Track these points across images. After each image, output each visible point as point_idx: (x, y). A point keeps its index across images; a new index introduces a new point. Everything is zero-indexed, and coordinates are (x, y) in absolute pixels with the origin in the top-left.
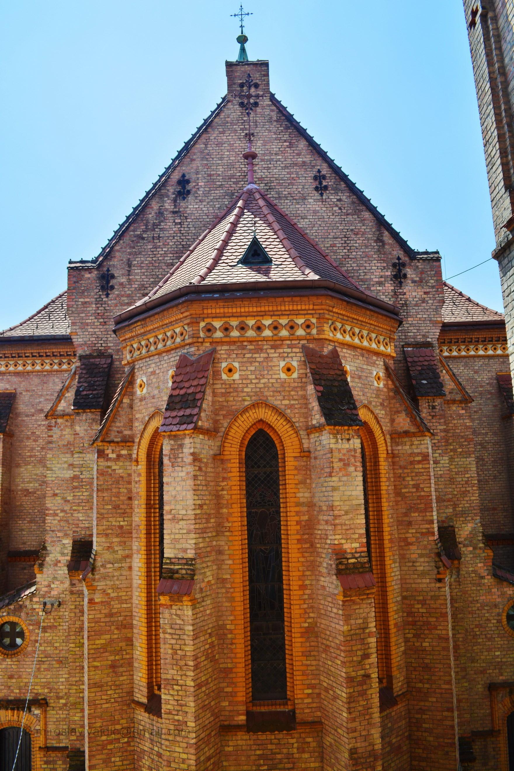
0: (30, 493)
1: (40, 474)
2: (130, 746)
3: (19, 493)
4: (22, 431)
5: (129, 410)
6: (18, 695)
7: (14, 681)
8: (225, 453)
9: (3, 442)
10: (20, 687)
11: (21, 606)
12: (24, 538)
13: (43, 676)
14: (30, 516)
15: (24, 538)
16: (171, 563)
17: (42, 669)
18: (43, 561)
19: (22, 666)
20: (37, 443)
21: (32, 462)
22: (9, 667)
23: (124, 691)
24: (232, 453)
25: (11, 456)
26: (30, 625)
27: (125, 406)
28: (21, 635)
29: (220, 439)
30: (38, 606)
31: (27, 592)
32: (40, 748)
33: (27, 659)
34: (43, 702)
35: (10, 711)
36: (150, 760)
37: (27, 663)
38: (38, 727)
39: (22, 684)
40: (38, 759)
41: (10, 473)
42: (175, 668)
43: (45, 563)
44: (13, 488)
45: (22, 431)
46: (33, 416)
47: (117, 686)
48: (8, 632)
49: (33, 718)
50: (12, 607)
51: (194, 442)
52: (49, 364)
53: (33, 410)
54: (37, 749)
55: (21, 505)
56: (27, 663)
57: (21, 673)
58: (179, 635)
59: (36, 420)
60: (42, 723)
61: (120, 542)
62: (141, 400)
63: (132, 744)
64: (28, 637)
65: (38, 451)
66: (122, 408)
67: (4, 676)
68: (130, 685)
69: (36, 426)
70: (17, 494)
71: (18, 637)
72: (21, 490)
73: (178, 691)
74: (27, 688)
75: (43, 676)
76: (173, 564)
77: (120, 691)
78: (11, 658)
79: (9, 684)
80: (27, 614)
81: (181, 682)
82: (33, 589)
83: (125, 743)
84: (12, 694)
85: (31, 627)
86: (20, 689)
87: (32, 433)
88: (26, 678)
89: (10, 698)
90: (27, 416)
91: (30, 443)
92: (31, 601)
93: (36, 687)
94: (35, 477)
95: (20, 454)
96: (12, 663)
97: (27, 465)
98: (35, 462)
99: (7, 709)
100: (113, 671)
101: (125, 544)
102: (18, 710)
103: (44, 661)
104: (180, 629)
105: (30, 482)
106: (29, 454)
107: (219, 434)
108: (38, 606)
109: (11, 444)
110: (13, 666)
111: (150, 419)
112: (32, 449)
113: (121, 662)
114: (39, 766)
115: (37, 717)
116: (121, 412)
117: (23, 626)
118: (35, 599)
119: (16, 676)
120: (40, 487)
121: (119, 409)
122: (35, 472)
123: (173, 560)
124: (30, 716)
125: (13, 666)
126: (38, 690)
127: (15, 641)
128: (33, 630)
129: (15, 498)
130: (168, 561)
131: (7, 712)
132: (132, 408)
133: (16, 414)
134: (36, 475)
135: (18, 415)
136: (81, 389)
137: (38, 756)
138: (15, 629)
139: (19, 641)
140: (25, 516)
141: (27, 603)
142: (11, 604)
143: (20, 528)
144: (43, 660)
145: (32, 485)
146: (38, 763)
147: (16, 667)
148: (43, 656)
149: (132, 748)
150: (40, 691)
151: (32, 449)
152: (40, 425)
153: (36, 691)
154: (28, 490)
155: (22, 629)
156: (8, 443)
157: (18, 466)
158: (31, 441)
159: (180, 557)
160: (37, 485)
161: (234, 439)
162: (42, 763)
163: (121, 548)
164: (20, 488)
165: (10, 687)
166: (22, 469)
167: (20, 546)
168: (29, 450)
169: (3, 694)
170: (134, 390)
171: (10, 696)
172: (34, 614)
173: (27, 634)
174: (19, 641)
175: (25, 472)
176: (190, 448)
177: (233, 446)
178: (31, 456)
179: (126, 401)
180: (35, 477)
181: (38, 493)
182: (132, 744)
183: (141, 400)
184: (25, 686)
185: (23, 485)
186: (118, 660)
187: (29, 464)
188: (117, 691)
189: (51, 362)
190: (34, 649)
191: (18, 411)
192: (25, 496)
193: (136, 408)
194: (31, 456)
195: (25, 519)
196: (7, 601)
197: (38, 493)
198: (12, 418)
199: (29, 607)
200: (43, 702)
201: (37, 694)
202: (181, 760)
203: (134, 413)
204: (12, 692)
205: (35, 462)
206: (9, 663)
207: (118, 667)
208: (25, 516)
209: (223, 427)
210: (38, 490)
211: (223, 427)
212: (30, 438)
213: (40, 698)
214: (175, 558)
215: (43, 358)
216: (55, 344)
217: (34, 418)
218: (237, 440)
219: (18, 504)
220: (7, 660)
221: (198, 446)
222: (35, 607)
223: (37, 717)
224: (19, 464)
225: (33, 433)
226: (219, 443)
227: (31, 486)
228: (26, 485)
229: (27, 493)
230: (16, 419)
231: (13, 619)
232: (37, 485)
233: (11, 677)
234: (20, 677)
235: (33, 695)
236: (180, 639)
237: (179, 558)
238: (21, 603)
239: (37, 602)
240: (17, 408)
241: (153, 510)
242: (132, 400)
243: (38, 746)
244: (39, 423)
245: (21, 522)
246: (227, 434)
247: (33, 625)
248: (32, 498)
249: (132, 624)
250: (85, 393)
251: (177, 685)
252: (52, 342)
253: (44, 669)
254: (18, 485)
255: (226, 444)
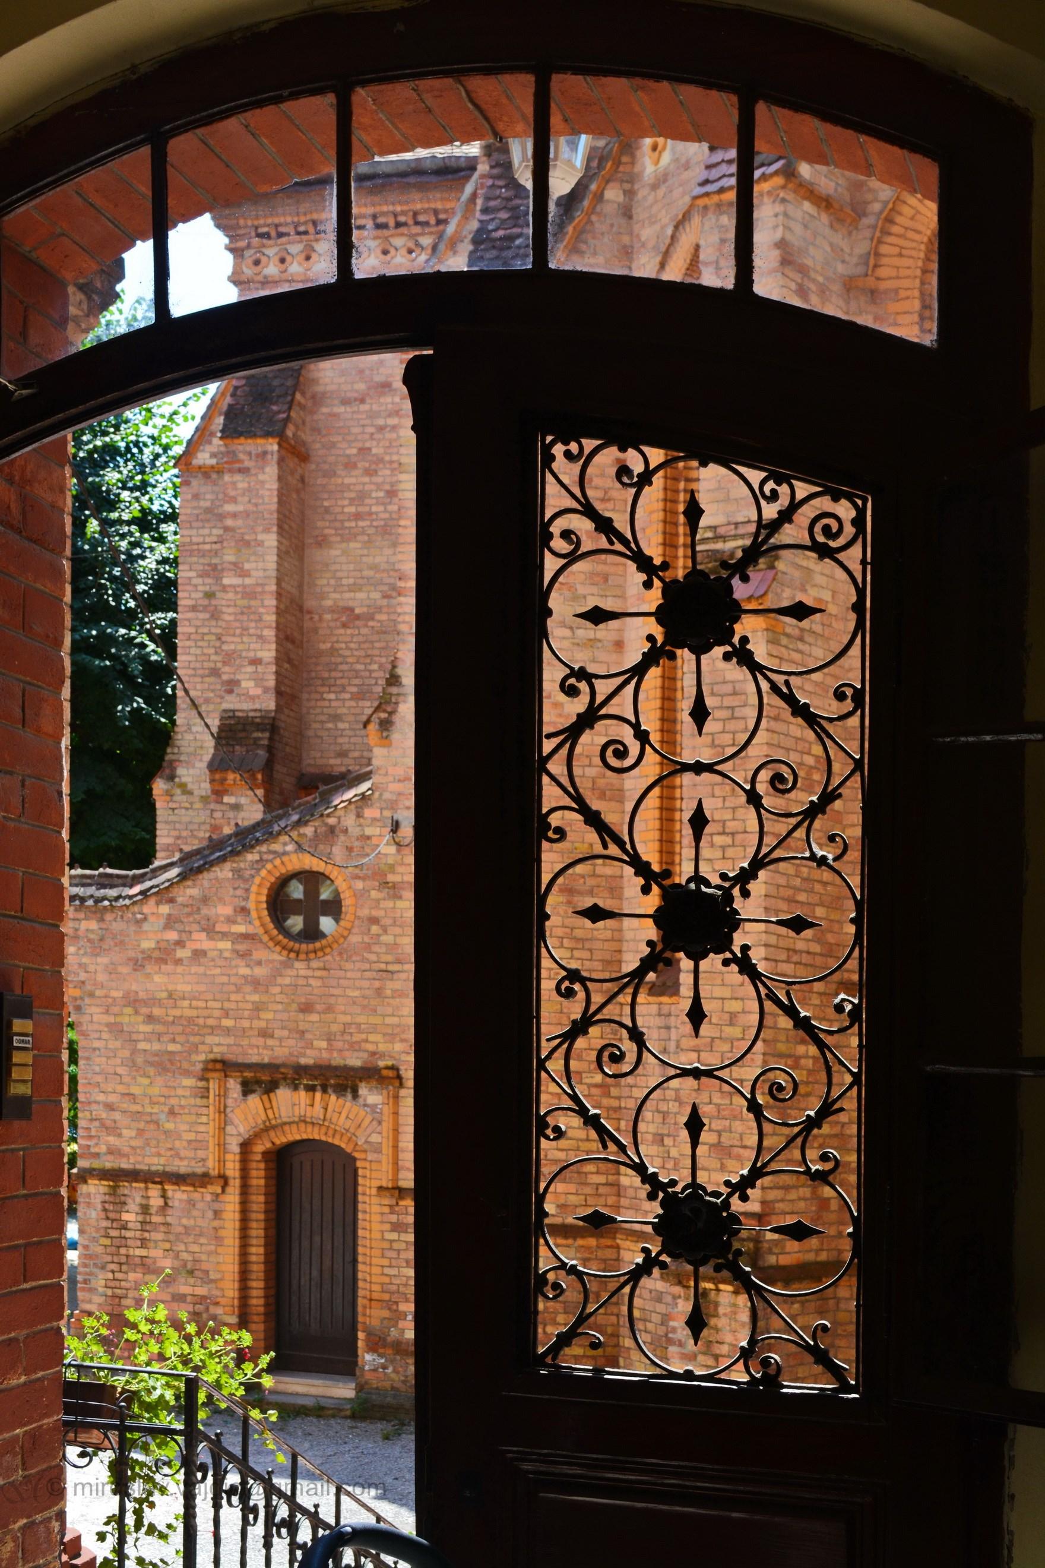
0: (358, 617)
1: (383, 566)
2: (608, 1095)
3: (328, 617)
4: (333, 445)
5: (623, 221)
6: (325, 1055)
7: (314, 1017)
8: (882, 272)
9: (279, 464)
10: (329, 1034)
11: (332, 830)
12: (340, 740)
13: (390, 1011)
14: (357, 681)
15: (340, 740)
16: (717, 538)
17: (388, 992)
18: (391, 713)
19: (334, 983)
20: (375, 479)
21: (363, 533)
22: (301, 982)
23: (598, 955)
24: (903, 272)
25: (302, 513)
26: (357, 877)
27: (609, 209)
28: (334, 908)
29: (868, 233)
30: (377, 831)
31: (349, 795)
32: (380, 1188)
33: (349, 966)
34: (390, 1073)
35: (302, 1093)
36: (658, 1118)
37: (349, 974)
38: (375, 1138)
39: (334, 1028)
40: (376, 1218)
41: (301, 559)
42: (717, 792)
43: (396, 718)
44: (310, 603)
45: (333, 445)
46: (362, 401)
47: (578, 940)
48: (299, 901)
49: (362, 1113)
50: (308, 831)
51: (786, 215)
52: (404, 251)
53: (361, 386)
54: (374, 1191)
55: (333, 651)
56: (349, 974)
57: (332, 1000)
58: (733, 708)
59: (372, 415)
60: (387, 1126)
61: (593, 574)
62: (655, 187)
63: (614, 1092)
64: (351, 910)
65: (379, 502)
66: (599, 214)
67: (289, 1004)
68: (614, 946)
69: (371, 430)
70: (321, 620)
71: (325, 914)
72: (332, 611)
73: (723, 848)
74: (347, 1037)
75: (390, 1011)
76: (724, 538)
77: (586, 955)
78: (308, 960)
79: (302, 1026)
80: (350, 849)
81: (731, 826)
82: (364, 787)
83: (596, 1086)
84: (308, 1052)
85: (359, 885)
86: (329, 1040)
87: (361, 450)
88: (344, 1013)
89: (303, 1061)
90: (345, 402)
91: (353, 479)
92: (359, 816)
93: (371, 1038)
94: (371, 573)
95: (327, 510)
96: (310, 973)
97: (349, 540)
98: (371, 531)
99: (296, 1088)
100: (569, 902)
101: (606, 580)
102: (324, 1090)
103: (392, 973)
104: (735, 693)
105: (354, 588)
106: (352, 509)
107: (866, 221)
108: (377, 831)
109: (302, 480)
110: (312, 981)
111: (676, 227)
112: (362, 496)
113: (591, 882)
114: (378, 1236)
115: (374, 1112)
116: (597, 225)
117: (341, 884)
118: (368, 813)
119: (318, 1007)
120: (385, 602)
121: (594, 218)
122: (369, 560)
123: (721, 531)
124: (355, 1109)
125: (312, 981)
126: (377, 1043)
127: (318, 923)
128: (366, 891)
129: (316, 631)
130: (709, 534)
131: (295, 1095)
132: (630, 217)
133: (313, 397)
134: (374, 567)
135: (317, 400)
136: (490, 227)
137: (376, 1209)
138: (318, 894)
139: (326, 923)
140: (345, 681)
141: (349, 821)
142: (306, 823)
143: (331, 711)
144: (390, 968)
145: (361, 595)
146: (376, 1227)
147: (319, 983)
148: (389, 958)
149: (615, 1103)
150: (382, 1047)
151: (362, 496)
152: (381, 429)
153: (371, 1047)
154: (352, 610)
155: (337, 893)
156: (292, 473)
157: (322, 542)
158: (355, 473)
159: (740, 519)
160: (376, 595)
161: (911, 234)
162: (388, 1227)
163: (594, 590)
164: (328, 603)
165: (303, 1032)
166: (334, 552)
167: (332, 762)
168: (352, 500)
169: (286, 1051)
170: (637, 169)
171: (304, 1055)
172: (367, 850)
173: (347, 901)
174: (326, 923)
175: (343, 559)
176: (776, 227)
177: (904, 252)
178: (358, 516)
179: (613, 194)
180: (371, 573)
181: (378, 617)
182: (614, 1092)
183: (655, 187)
184: (344, 1032)
185: (337, 596)
186: (583, 877)
187: (353, 537)
188: (576, 954)
189: (411, 245)
190: (367, 939)
191: (320, 389)
192: (344, 626)
193: (639, 213)
194: (358, 516)
195: (343, 689)
196: (295, 817)
197: (378, 617)
198: (302, 407)
199: (354, 831)
200: (390, 1073)
201: (373, 1054)
202: (727, 1017)
203: (636, 228)
204: (310, 1045)
205: (371, 531)
206: (302, 973)
207: (581, 893)
208: (345, 681)
209: (876, 200)
210: (379, 609)
211: (876, 200)
212: (354, 466)
213: (381, 1064)
214: (729, 524)
215: (386, 232)
216: (421, 187)
217: (364, 407)
218: (917, 237)
219: (323, 646)
220: (297, 965)
221: (798, 229)
222: (368, 831)
223: (374, 1112)
224: (325, 536)
225: (364, 451)
226: (863, 247)
227: (360, 600)
228: (347, 595)
229: (349, 616)
230: (312, 412)
231: (310, 862)
232: (376, 595)
233: (306, 1008)
234: (329, 1009)
235: (365, 1055)
236: (733, 718)
237: (736, 524)
238: (332, 821)
239: (374, 820)
240: (315, 381)
241: (682, 485)
242: (630, 194)
243: (376, 1184)
244: (381, 422)
245: (332, 696)
246: (889, 220)
247: (363, 878)
248: (364, 631)
249: (622, 790)
250: (501, 233)
251: (723, 833)
252: (412, 180)
253: (394, 991)
254: (323, 596)
255: (884, 249)
